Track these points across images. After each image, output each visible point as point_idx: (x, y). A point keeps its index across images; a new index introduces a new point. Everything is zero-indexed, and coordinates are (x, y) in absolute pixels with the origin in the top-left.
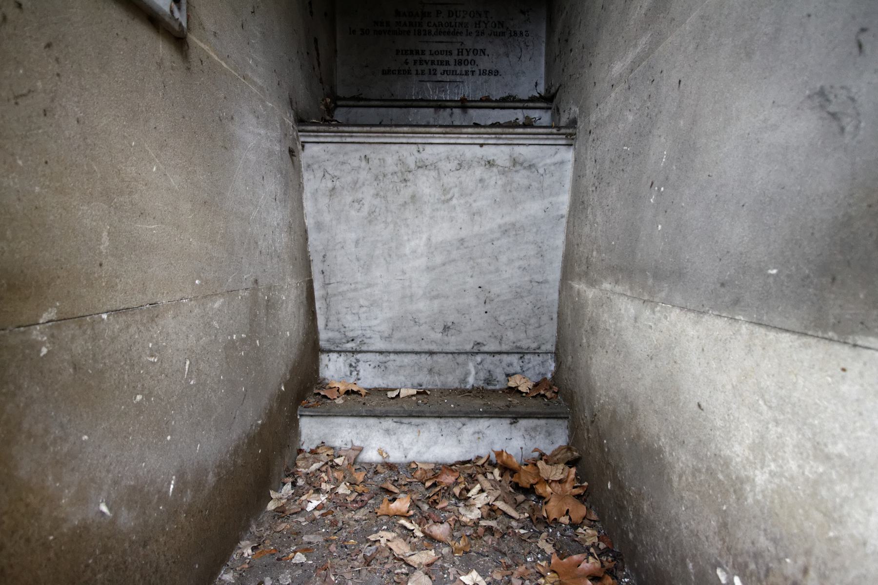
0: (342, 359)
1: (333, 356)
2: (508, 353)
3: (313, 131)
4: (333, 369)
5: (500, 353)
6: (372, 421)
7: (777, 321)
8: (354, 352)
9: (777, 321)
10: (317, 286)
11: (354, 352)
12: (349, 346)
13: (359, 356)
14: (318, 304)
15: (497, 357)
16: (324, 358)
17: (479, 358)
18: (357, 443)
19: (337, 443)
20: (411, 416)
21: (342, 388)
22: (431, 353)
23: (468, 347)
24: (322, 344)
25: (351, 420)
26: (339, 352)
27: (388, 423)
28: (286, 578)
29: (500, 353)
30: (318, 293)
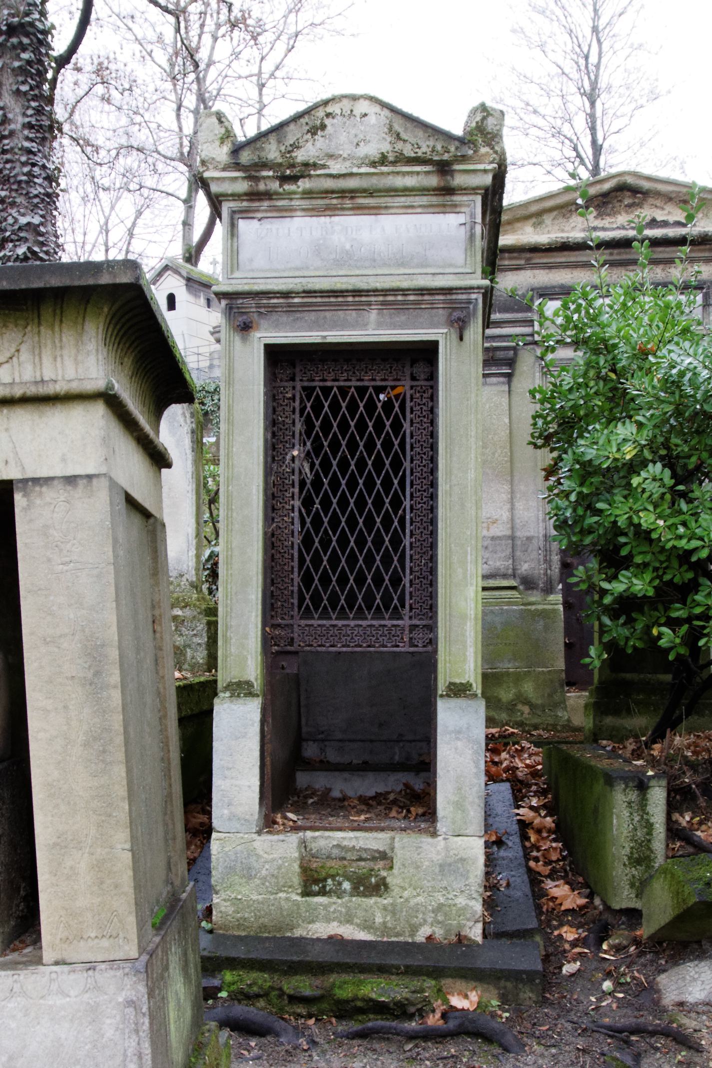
0: (316, 745)
1: (311, 743)
2: (419, 741)
3: (355, 298)
4: (310, 750)
5: (414, 741)
6: (337, 773)
7: (268, 747)
8: (323, 740)
9: (268, 747)
10: (302, 698)
11: (323, 740)
12: (320, 736)
13: (327, 743)
14: (302, 710)
15: (414, 744)
16: (304, 744)
17: (401, 744)
18: (328, 786)
19: (317, 787)
20: (358, 770)
21: (318, 760)
22: (372, 741)
23: (395, 737)
24: (304, 735)
25: (325, 773)
26: (314, 741)
27: (346, 775)
28: (423, 1067)
29: (414, 741)
30: (303, 703)
